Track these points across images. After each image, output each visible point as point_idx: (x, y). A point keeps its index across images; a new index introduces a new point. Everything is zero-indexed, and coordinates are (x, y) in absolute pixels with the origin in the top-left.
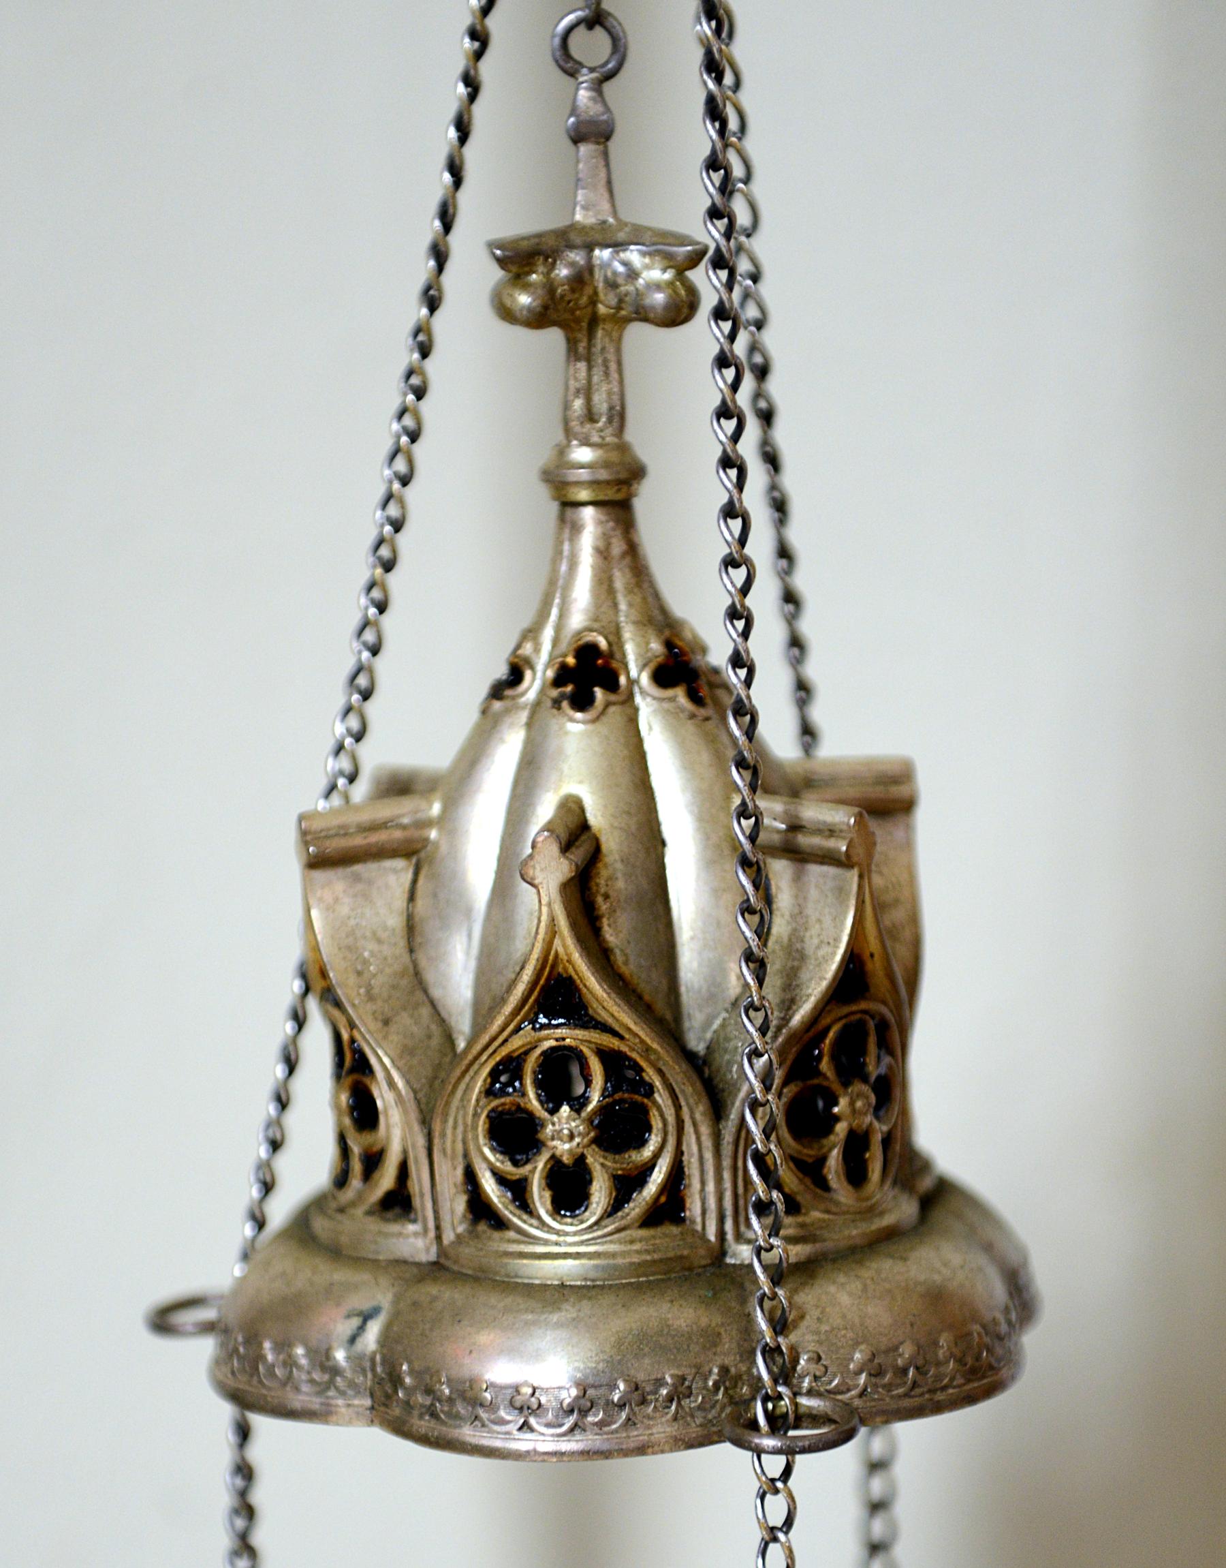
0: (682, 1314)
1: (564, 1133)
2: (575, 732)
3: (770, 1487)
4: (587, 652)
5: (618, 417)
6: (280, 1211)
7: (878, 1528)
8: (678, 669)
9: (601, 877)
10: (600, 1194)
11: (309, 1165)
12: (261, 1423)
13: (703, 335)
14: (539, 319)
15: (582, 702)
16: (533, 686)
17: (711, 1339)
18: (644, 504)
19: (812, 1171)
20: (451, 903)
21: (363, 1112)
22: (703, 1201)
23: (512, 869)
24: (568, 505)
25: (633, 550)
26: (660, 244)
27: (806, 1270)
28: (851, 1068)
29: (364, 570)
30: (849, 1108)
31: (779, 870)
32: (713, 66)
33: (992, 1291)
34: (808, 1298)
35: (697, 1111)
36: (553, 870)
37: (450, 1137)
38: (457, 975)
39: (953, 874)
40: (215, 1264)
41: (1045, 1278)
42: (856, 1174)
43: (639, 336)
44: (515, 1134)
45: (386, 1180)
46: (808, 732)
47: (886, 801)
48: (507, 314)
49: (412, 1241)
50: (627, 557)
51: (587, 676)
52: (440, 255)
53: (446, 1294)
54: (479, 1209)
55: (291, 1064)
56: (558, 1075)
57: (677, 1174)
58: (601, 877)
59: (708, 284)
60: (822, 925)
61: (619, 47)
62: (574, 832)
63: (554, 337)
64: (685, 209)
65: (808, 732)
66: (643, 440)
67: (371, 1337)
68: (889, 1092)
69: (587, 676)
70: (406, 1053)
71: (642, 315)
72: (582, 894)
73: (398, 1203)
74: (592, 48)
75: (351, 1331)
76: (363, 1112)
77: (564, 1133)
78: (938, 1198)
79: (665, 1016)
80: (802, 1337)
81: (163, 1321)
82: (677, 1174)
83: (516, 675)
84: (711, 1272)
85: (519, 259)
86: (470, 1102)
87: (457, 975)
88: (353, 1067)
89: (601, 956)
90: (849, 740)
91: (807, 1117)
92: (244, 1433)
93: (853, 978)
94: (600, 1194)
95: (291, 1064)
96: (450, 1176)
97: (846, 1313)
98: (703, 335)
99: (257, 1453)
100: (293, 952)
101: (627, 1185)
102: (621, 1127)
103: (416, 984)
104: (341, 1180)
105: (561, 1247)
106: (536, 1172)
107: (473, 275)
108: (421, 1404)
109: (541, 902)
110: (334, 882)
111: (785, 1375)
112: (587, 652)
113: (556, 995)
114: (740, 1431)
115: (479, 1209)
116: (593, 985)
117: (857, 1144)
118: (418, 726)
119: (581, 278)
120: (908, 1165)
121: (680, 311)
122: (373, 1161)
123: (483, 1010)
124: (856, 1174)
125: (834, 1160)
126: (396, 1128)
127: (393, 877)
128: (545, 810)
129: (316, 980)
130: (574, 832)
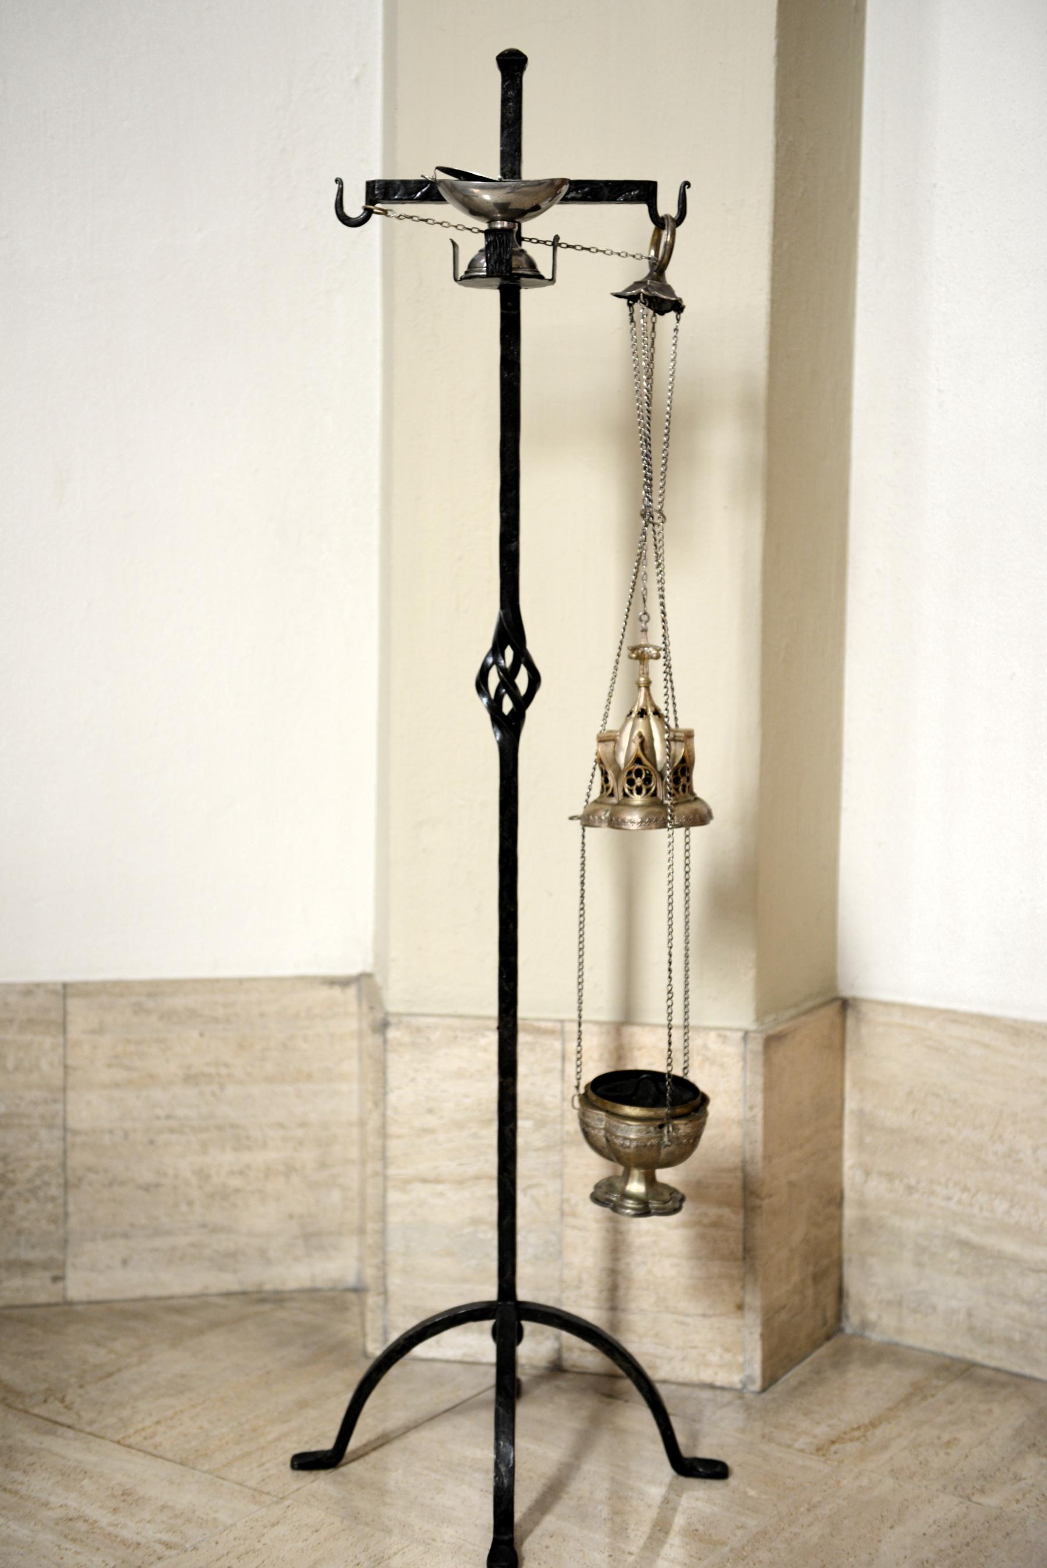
0: (657, 809)
1: (639, 782)
2: (641, 720)
3: (669, 999)
4: (643, 710)
5: (648, 673)
6: (591, 800)
7: (687, 869)
8: (656, 712)
9: (645, 744)
10: (644, 791)
11: (596, 793)
12: (587, 829)
13: (662, 661)
14: (636, 658)
15: (642, 717)
16: (633, 715)
17: (661, 813)
18: (652, 687)
19: (677, 790)
20: (620, 748)
21: (606, 781)
22: (660, 794)
23: (631, 741)
24: (639, 687)
25: (650, 695)
26: (655, 648)
27: (675, 805)
28: (683, 774)
29: (606, 697)
30: (683, 780)
31: (672, 743)
32: (663, 621)
33: (705, 811)
34: (676, 808)
35: (659, 779)
36: (638, 741)
37: (620, 783)
38: (622, 759)
39: (699, 745)
40: (580, 812)
41: (714, 813)
42: (684, 791)
43: (651, 662)
44: (631, 782)
45: (610, 791)
46: (677, 725)
47: (689, 735)
48: (630, 658)
49: (614, 800)
50: (648, 695)
51: (642, 713)
52: (620, 648)
53: (620, 808)
54: (625, 795)
55: (593, 776)
56: (638, 773)
57: (656, 790)
58: (645, 744)
59: (662, 653)
60: (680, 751)
61: (649, 617)
62: (641, 736)
63: (638, 662)
64: (659, 642)
65: (677, 725)
66: (651, 677)
67: (608, 815)
68: (689, 779)
69: (642, 713)
70: (614, 771)
71: (652, 658)
72: (642, 744)
73: (612, 795)
74: (645, 618)
75: (604, 815)
76: (606, 781)
77: (639, 782)
78: (696, 799)
79: (654, 763)
80: (675, 813)
81: (571, 818)
82: (656, 790)
83: (631, 713)
84: (661, 804)
85: (633, 649)
86: (624, 777)
87: (622, 759)
88: (604, 774)
89: (645, 755)
90: (683, 725)
91: (676, 781)
92: (584, 830)
93: (683, 760)
94: (644, 791)
95: (593, 776)
96: (620, 789)
97: (683, 810)
98: (662, 661)
99: (586, 833)
100: (595, 757)
101: (648, 790)
102: (648, 780)
103: (615, 761)
104: (602, 792)
105: (637, 799)
106: (634, 788)
107: (625, 652)
108: (615, 823)
109: (635, 747)
110: (601, 745)
111: (672, 818)
112: (643, 710)
113: (638, 760)
114: (663, 825)
115: (625, 795)
116: (643, 759)
117: (684, 786)
118: (612, 725)
119: (643, 652)
120: (692, 793)
121: (658, 657)
122: (608, 788)
123: (626, 764)
124: (684, 791)
125: (680, 789)
126: (612, 782)
127: (611, 744)
128: (636, 733)
129: (600, 761)
130: (641, 736)
